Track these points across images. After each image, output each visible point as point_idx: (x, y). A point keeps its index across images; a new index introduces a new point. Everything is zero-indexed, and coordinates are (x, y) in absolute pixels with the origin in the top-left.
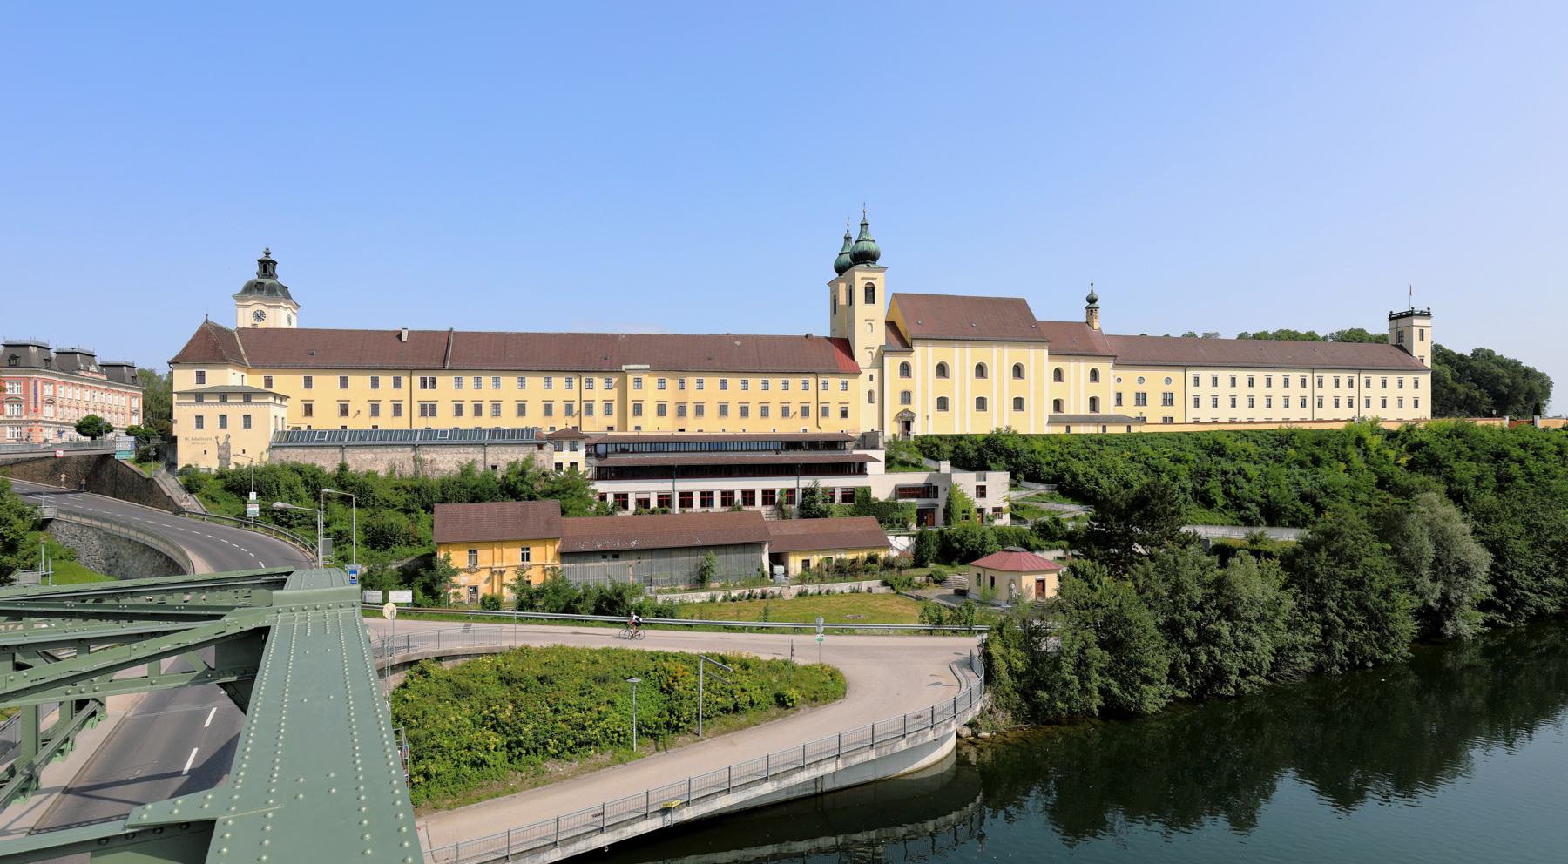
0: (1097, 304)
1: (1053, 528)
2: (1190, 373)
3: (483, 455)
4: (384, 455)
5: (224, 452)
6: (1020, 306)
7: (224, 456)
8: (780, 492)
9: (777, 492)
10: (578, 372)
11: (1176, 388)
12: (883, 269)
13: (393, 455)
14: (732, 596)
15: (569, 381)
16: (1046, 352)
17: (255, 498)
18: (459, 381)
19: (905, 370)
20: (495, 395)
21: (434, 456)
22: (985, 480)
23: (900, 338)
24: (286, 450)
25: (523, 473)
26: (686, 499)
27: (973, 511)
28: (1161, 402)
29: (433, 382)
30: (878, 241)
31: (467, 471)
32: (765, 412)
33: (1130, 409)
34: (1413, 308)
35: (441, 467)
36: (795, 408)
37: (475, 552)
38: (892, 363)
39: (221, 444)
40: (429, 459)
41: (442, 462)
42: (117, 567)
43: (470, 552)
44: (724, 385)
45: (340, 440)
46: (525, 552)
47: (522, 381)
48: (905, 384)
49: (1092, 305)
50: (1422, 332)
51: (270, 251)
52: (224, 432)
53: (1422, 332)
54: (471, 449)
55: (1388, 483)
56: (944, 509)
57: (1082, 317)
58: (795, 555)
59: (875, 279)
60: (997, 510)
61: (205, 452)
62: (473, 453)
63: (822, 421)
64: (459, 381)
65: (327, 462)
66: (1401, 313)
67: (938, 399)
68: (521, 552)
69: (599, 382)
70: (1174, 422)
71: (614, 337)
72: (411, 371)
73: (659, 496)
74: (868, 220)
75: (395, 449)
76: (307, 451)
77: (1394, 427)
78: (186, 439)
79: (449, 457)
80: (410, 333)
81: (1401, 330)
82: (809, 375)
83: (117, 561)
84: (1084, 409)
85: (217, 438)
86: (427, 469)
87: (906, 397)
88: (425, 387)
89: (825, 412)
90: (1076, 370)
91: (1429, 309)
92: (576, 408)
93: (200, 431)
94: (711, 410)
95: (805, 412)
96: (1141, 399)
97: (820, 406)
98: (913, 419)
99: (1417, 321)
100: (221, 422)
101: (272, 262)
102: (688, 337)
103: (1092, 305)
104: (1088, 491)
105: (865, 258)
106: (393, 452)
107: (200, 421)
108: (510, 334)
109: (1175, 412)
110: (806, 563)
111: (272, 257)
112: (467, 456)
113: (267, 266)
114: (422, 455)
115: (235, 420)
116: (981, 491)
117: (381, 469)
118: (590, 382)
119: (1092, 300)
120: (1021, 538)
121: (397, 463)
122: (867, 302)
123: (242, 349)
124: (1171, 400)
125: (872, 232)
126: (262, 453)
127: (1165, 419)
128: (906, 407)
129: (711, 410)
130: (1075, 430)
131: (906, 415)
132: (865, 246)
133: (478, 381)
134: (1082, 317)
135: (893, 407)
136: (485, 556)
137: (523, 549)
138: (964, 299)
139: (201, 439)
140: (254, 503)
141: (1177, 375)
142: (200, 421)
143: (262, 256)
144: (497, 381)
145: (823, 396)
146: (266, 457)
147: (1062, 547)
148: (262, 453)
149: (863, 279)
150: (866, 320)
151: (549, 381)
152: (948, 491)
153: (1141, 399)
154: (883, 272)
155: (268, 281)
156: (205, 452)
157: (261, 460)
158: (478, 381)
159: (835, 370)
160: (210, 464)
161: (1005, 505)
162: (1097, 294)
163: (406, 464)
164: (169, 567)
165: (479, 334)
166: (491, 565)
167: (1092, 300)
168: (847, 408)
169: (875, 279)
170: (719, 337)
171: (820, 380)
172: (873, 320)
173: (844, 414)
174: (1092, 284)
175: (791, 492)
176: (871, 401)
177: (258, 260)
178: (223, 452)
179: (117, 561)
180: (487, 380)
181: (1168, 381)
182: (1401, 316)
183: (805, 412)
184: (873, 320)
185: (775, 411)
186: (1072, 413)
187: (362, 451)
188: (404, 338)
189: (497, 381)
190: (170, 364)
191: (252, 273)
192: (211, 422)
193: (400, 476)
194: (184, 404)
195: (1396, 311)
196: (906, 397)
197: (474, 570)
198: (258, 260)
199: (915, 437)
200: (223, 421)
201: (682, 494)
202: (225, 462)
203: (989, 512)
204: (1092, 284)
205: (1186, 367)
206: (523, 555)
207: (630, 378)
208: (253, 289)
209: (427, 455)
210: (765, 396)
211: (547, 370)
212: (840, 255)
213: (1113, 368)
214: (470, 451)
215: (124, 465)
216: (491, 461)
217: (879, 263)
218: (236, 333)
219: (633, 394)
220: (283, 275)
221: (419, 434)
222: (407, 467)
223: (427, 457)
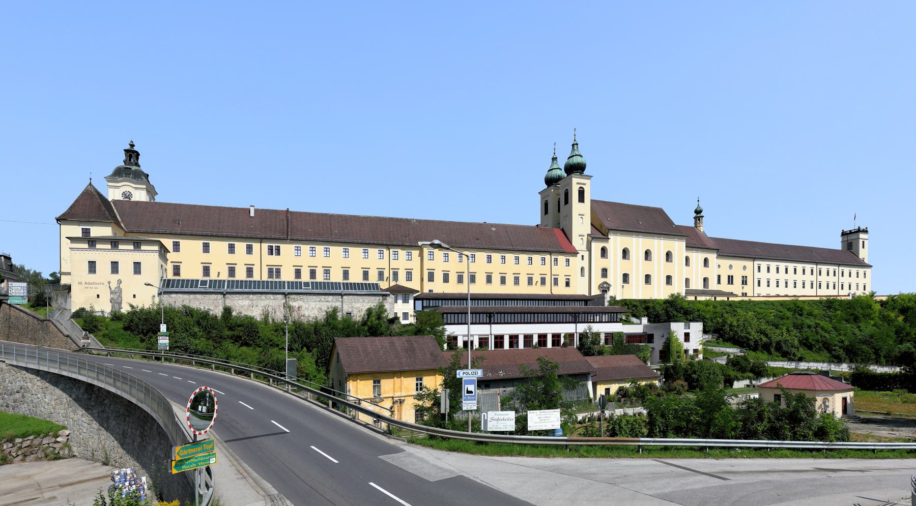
0: (702, 214)
1: (744, 363)
2: (756, 263)
3: (340, 304)
4: (259, 302)
5: (116, 296)
6: (660, 212)
7: (116, 301)
8: (565, 335)
9: (562, 336)
10: (388, 246)
11: (748, 273)
12: (589, 177)
13: (266, 302)
14: (579, 420)
15: (381, 253)
16: (684, 243)
17: (165, 331)
18: (298, 249)
19: (604, 252)
20: (327, 262)
21: (300, 303)
22: (689, 329)
23: (600, 231)
24: (173, 295)
25: (379, 317)
26: (499, 340)
27: (683, 352)
28: (741, 283)
29: (278, 249)
30: (586, 157)
31: (332, 315)
32: (517, 281)
33: (725, 287)
34: (859, 227)
35: (307, 313)
36: (537, 278)
37: (379, 382)
38: (597, 246)
39: (113, 289)
40: (297, 306)
41: (307, 309)
42: (23, 402)
43: (374, 382)
44: (489, 259)
45: (216, 288)
46: (419, 382)
47: (346, 251)
48: (603, 263)
49: (699, 215)
50: (863, 242)
51: (134, 143)
52: (115, 277)
53: (863, 242)
54: (330, 298)
55: (902, 333)
56: (661, 352)
57: (691, 223)
58: (600, 384)
59: (585, 184)
60: (696, 351)
61: (98, 296)
62: (333, 301)
63: (472, 286)
64: (298, 249)
65: (213, 306)
66: (850, 231)
67: (623, 274)
68: (415, 382)
69: (402, 253)
70: (748, 295)
71: (408, 221)
72: (261, 240)
73: (480, 339)
74: (578, 141)
75: (268, 296)
76: (192, 296)
77: (884, 299)
78: (80, 283)
79: (313, 304)
80: (256, 210)
81: (851, 241)
82: (545, 253)
83: (23, 396)
84: (225, 276)
85: (109, 283)
86: (295, 315)
87: (604, 272)
88: (272, 254)
89: (556, 282)
90: (697, 257)
91: (866, 228)
92: (386, 275)
93: (92, 275)
94: (481, 278)
95: (543, 282)
96: (730, 280)
97: (553, 277)
98: (609, 288)
99: (862, 236)
100: (112, 268)
101: (137, 152)
102: (459, 223)
103: (699, 215)
104: (742, 338)
105: (576, 169)
106: (266, 298)
107: (92, 266)
108: (332, 215)
109: (748, 289)
110: (608, 390)
111: (135, 149)
112: (328, 304)
113: (132, 154)
114: (291, 303)
115: (126, 267)
116: (687, 337)
117: (256, 314)
118: (396, 253)
119: (698, 212)
120: (723, 371)
121: (270, 309)
122: (579, 201)
123: (118, 217)
124: (746, 281)
125: (581, 150)
126: (154, 296)
127: (743, 294)
128: (604, 280)
129: (481, 278)
130: (700, 298)
131: (605, 285)
132: (577, 160)
133: (313, 250)
134: (691, 223)
135: (597, 280)
136: (387, 385)
137: (417, 380)
138: (628, 205)
139: (95, 284)
140: (164, 335)
141: (749, 264)
142: (92, 266)
143: (128, 147)
144: (327, 250)
145: (555, 270)
146: (157, 300)
147: (749, 378)
148: (154, 296)
149: (578, 183)
150: (579, 215)
151: (365, 252)
152: (665, 337)
153: (730, 280)
154: (589, 179)
155: (134, 168)
156: (98, 296)
157: (153, 303)
158: (313, 250)
159: (561, 250)
160: (103, 307)
161: (700, 348)
162: (702, 207)
163: (277, 310)
164: (90, 399)
165: (309, 214)
166: (392, 395)
167: (698, 212)
168: (569, 279)
169: (585, 184)
170: (480, 225)
171: (553, 257)
172: (583, 215)
173: (568, 284)
174: (698, 201)
175: (570, 336)
176: (582, 275)
177: (125, 150)
178: (115, 297)
179: (23, 396)
180: (320, 249)
181: (745, 268)
182: (851, 232)
183: (543, 282)
184: (583, 215)
185: (523, 280)
186: (694, 288)
187: (240, 298)
188: (252, 214)
189: (327, 250)
190: (58, 220)
191: (120, 160)
192: (103, 267)
193: (273, 320)
194: (78, 249)
195: (847, 229)
196: (604, 272)
197: (377, 400)
198: (125, 150)
199: (613, 299)
200: (115, 266)
201: (496, 337)
202: (117, 306)
203: (691, 352)
204: (698, 201)
205: (754, 259)
206: (417, 384)
207: (426, 251)
208: (119, 174)
209: (295, 303)
210: (516, 269)
211: (365, 244)
212: (549, 171)
213: (688, 247)
214: (323, 299)
215: (17, 309)
216: (346, 308)
217: (585, 173)
218: (112, 203)
219: (428, 265)
220: (145, 164)
221: (286, 284)
222: (278, 313)
223: (295, 304)
